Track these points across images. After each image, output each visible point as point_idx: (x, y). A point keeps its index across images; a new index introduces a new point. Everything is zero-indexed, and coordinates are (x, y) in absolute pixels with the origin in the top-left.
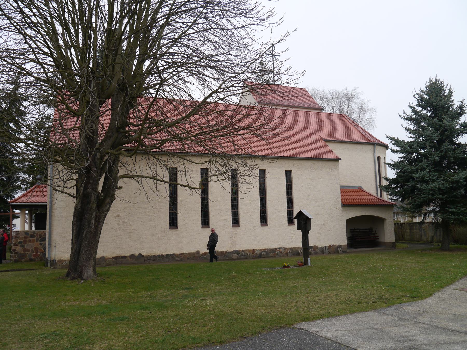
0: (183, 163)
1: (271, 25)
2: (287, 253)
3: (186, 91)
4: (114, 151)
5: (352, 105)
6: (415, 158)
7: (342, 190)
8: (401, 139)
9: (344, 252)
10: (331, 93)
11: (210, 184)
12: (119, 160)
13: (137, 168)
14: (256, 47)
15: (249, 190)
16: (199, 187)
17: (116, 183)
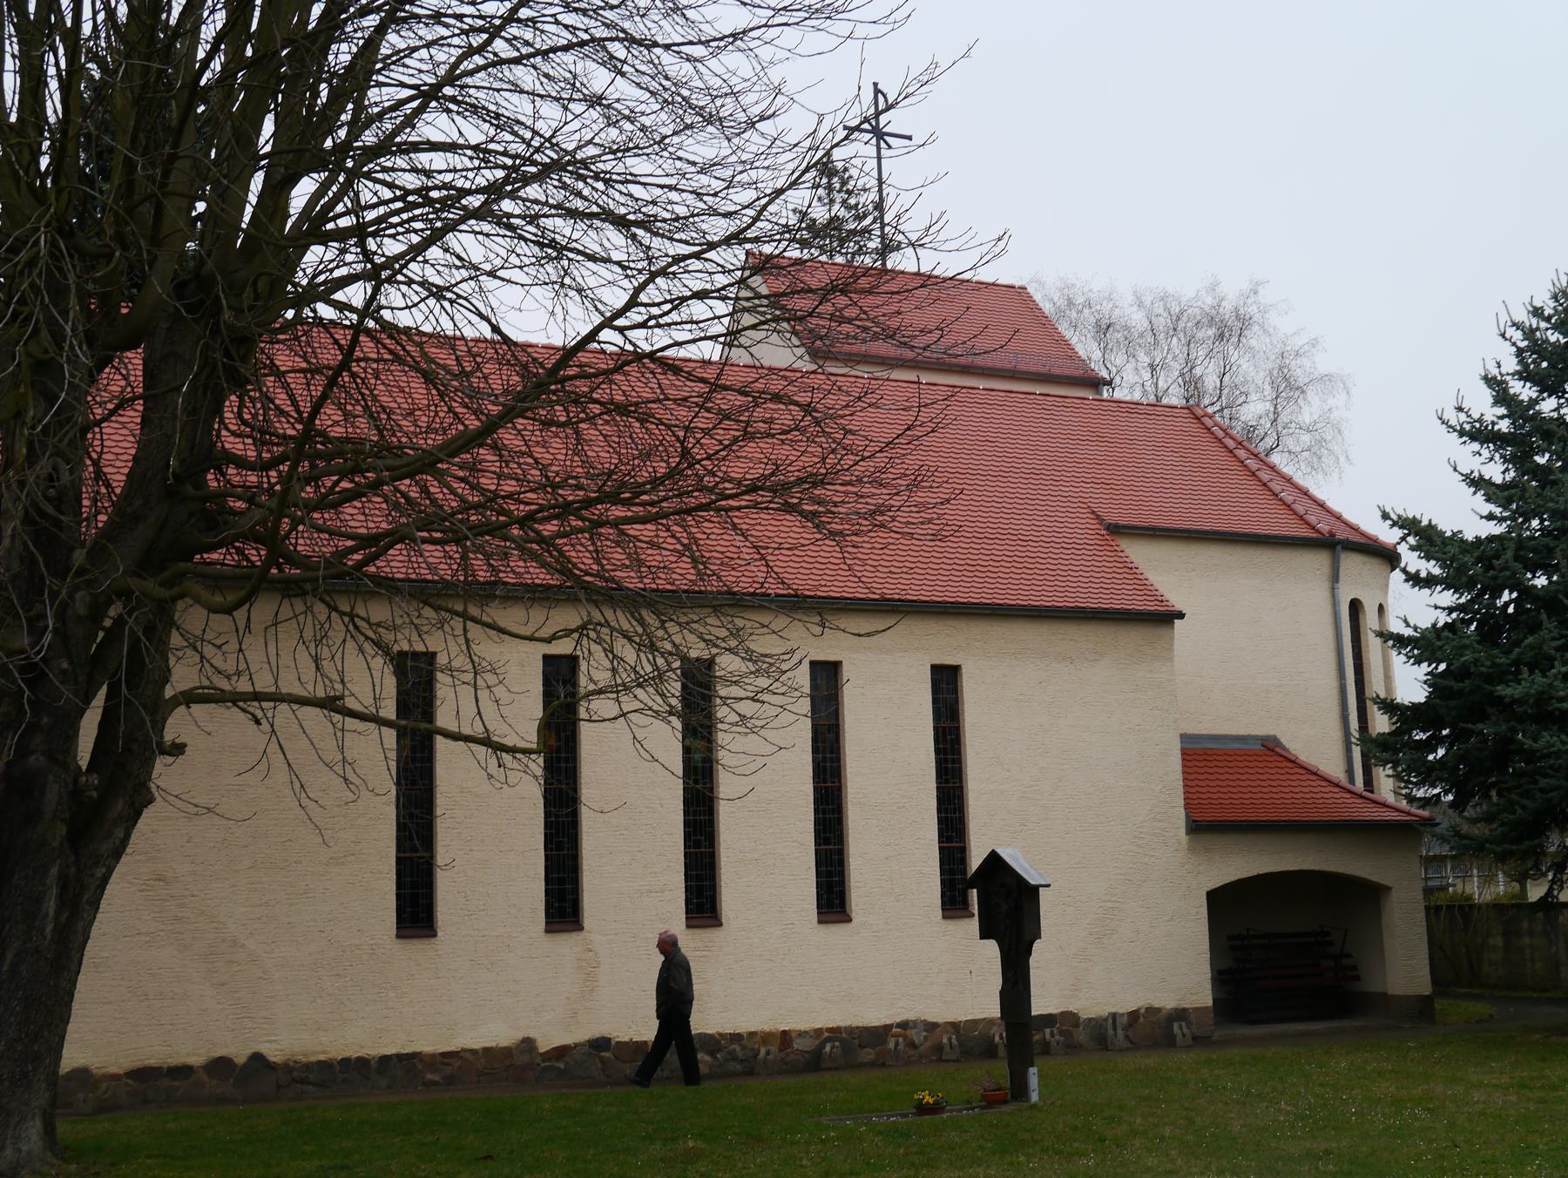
0: (467, 641)
1: (861, 31)
2: (939, 1048)
3: (483, 310)
4: (152, 586)
5: (1241, 361)
6: (1511, 610)
7: (1185, 754)
8: (1447, 526)
9: (1199, 1041)
10: (1148, 303)
11: (587, 732)
12: (171, 624)
13: (255, 655)
14: (795, 125)
15: (761, 761)
16: (534, 746)
17: (160, 726)
